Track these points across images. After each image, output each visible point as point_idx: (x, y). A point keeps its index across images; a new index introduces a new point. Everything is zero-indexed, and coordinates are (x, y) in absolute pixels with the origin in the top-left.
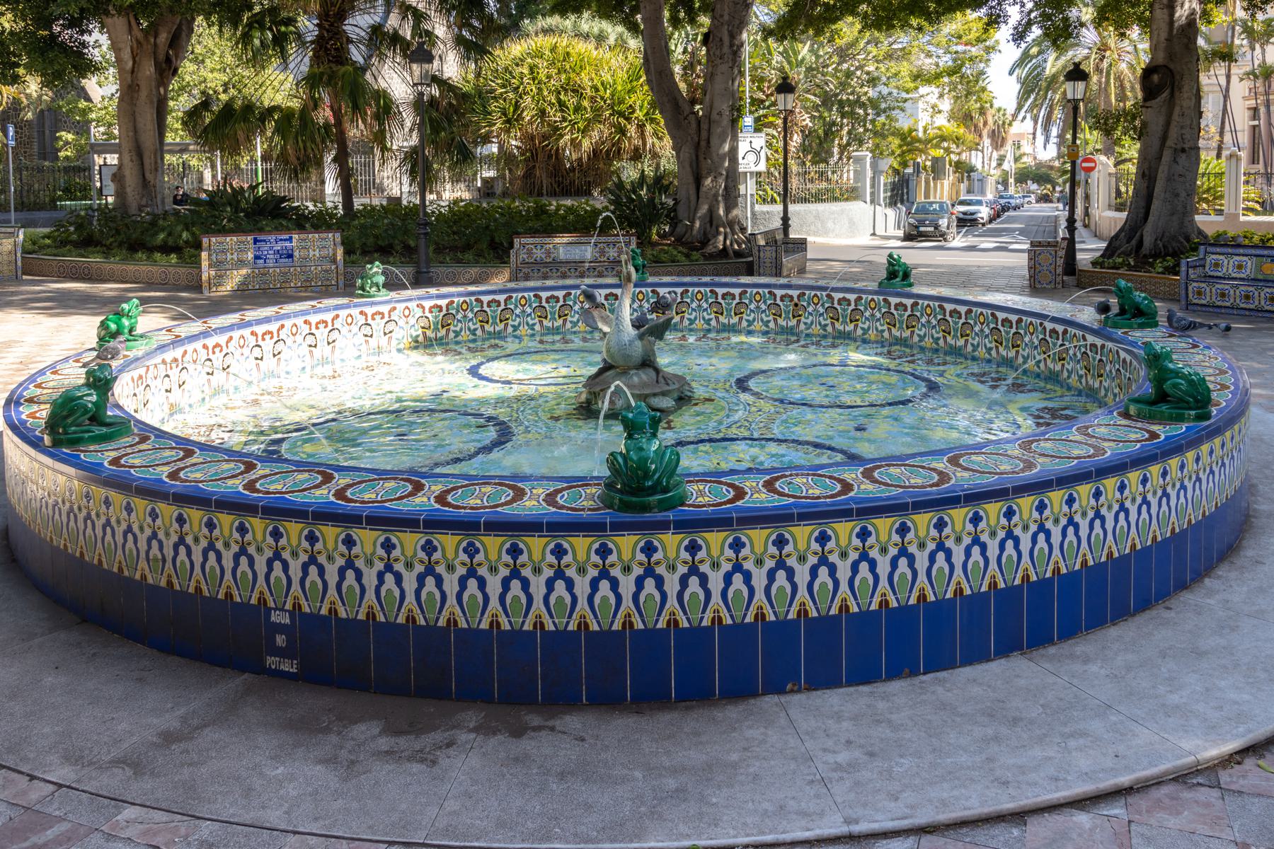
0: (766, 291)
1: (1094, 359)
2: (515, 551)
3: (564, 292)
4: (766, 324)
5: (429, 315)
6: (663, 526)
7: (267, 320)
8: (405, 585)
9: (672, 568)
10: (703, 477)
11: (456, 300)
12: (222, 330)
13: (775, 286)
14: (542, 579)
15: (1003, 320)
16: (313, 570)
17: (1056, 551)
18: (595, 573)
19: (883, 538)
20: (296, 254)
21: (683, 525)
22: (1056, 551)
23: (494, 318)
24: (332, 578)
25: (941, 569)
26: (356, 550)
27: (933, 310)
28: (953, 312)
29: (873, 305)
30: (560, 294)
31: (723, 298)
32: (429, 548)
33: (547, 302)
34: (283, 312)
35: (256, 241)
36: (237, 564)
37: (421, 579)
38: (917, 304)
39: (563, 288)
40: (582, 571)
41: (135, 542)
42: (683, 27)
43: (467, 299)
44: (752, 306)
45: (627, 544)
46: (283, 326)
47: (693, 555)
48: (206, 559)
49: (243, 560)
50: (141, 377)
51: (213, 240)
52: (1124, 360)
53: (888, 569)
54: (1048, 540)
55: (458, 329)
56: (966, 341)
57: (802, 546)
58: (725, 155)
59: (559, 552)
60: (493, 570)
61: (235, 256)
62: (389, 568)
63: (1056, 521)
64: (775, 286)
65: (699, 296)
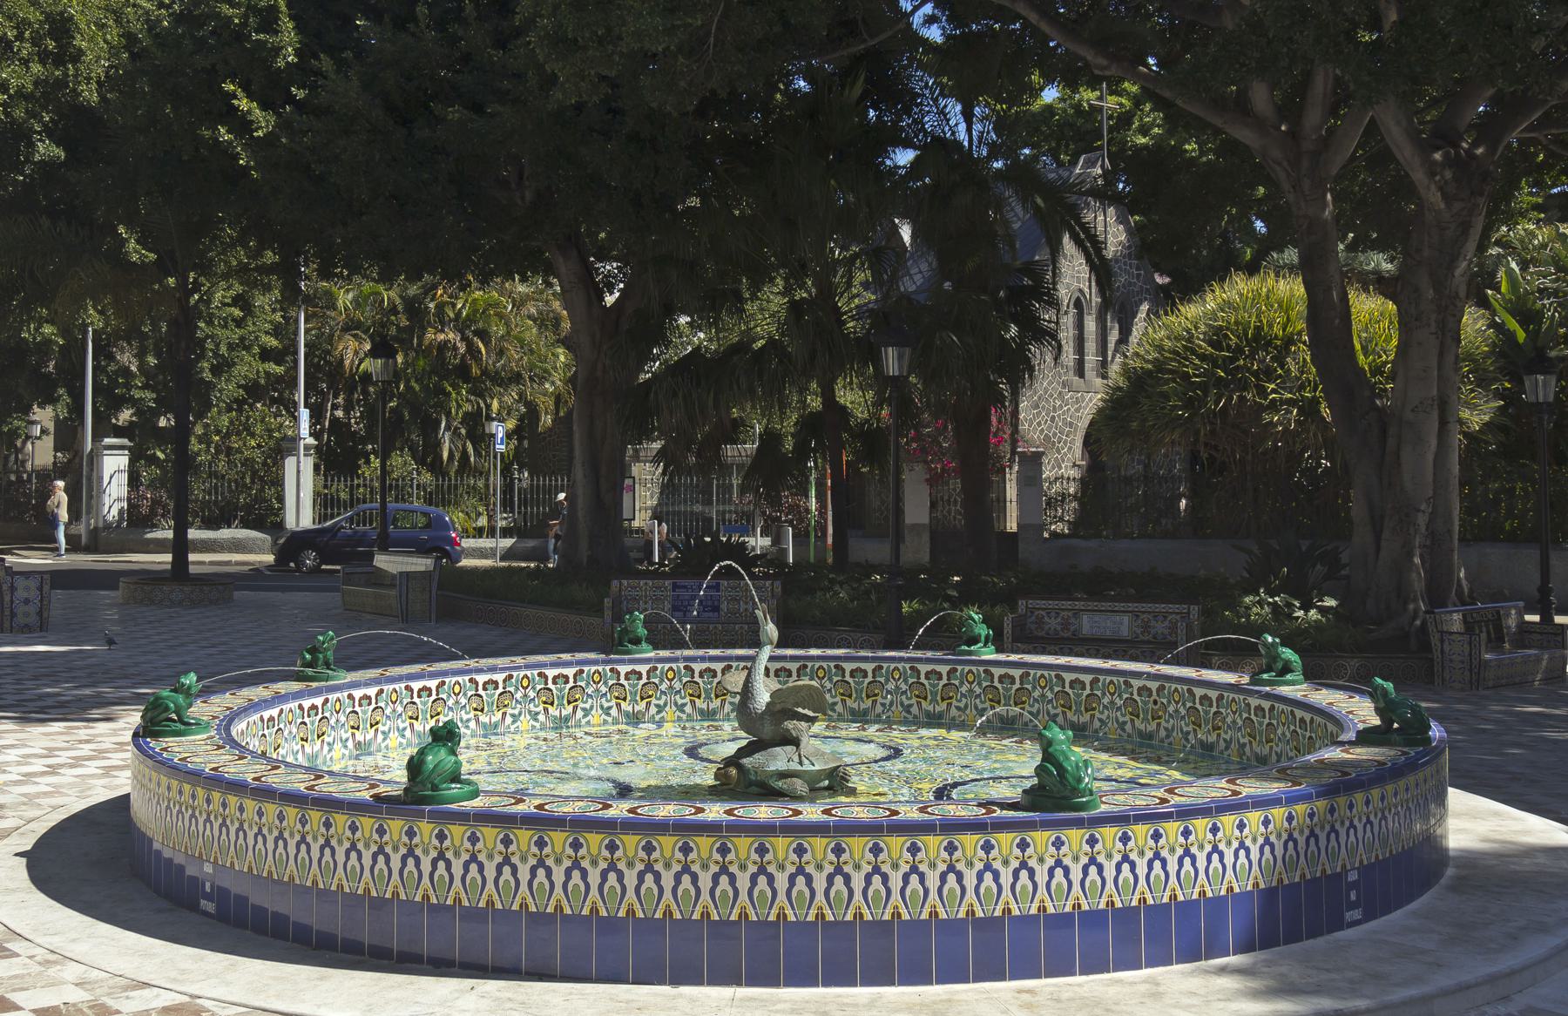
0: (908, 666)
3: (873, 665)
4: (907, 709)
5: (850, 680)
6: (421, 815)
8: (1002, 880)
9: (705, 867)
10: (1460, 831)
11: (515, 674)
13: (544, 665)
14: (748, 875)
16: (381, 858)
17: (1229, 871)
18: (679, 868)
20: (724, 606)
22: (1229, 871)
23: (934, 694)
27: (1182, 696)
28: (1204, 698)
29: (457, 689)
30: (869, 667)
31: (927, 678)
33: (627, 678)
35: (675, 587)
36: (375, 861)
37: (533, 871)
38: (805, 667)
39: (874, 659)
40: (970, 864)
41: (285, 847)
42: (65, 66)
44: (663, 687)
45: (396, 826)
48: (348, 858)
49: (381, 858)
51: (625, 582)
53: (1081, 876)
54: (1248, 856)
55: (661, 702)
56: (1159, 725)
58: (45, 478)
64: (919, 660)
65: (670, 675)
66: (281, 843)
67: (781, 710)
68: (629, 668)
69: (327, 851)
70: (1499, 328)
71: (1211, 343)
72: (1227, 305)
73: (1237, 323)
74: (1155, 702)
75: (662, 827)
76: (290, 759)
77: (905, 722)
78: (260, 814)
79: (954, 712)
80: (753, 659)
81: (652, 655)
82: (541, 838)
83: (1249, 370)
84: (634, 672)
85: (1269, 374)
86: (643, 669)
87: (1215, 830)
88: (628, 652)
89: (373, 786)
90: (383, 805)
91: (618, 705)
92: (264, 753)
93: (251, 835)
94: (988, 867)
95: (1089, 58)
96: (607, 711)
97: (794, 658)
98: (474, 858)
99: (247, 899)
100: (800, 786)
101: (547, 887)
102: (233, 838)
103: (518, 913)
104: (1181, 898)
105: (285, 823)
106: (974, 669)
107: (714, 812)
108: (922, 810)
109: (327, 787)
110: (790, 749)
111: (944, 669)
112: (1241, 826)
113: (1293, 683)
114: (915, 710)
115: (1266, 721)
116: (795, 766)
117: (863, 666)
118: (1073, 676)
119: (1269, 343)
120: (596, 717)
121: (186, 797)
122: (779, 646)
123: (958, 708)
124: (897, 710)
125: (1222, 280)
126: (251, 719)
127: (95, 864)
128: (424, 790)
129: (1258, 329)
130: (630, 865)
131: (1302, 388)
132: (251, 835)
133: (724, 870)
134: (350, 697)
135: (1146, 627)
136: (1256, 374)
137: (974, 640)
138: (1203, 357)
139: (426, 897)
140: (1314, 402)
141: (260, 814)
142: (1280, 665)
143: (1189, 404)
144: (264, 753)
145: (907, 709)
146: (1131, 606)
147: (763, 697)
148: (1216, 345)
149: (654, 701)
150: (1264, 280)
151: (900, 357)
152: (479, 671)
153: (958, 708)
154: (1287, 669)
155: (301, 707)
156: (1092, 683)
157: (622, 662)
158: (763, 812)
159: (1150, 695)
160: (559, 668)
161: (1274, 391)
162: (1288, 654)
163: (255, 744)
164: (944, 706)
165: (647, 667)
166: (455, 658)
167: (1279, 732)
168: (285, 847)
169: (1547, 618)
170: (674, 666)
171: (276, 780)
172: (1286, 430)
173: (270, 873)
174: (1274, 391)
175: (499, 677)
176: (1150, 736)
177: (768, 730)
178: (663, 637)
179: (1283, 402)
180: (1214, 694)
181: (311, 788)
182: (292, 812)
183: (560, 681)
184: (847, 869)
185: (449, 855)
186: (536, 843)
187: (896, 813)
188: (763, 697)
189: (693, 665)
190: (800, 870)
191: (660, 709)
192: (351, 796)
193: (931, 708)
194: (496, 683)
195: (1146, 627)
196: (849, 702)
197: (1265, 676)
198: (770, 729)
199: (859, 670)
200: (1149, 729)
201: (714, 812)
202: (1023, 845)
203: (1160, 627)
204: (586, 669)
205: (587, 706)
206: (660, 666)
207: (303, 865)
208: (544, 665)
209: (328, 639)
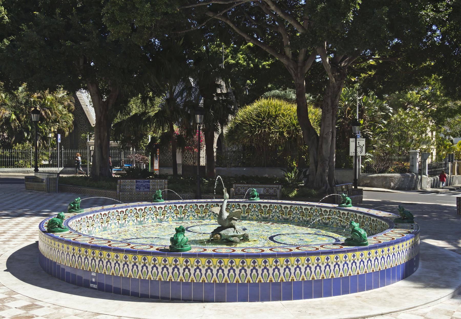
0: (173, 205)
1: (374, 224)
2: (145, 259)
3: (206, 204)
6: (179, 255)
7: (122, 207)
11: (147, 207)
12: (107, 210)
13: (136, 206)
15: (342, 213)
16: (126, 266)
19: (292, 262)
20: (151, 187)
21: (184, 255)
23: (265, 212)
24: (105, 264)
25: (318, 271)
26: (127, 259)
28: (325, 211)
29: (276, 207)
30: (183, 205)
31: (158, 209)
32: (126, 258)
33: (179, 208)
34: (116, 207)
35: (137, 182)
36: (133, 267)
37: (163, 269)
39: (185, 203)
41: (81, 260)
43: (151, 207)
45: (170, 259)
46: (127, 210)
47: (176, 263)
49: (126, 266)
50: (79, 221)
51: (122, 181)
52: (383, 224)
54: (356, 265)
57: (303, 262)
59: (155, 260)
60: (248, 267)
61: (129, 187)
62: (117, 262)
63: (350, 261)
64: (240, 202)
66: (80, 258)
67: (230, 218)
68: (159, 206)
69: (93, 261)
70: (222, 128)
71: (256, 116)
72: (261, 106)
73: (263, 111)
74: (309, 212)
75: (225, 256)
76: (84, 233)
77: (256, 220)
78: (80, 251)
79: (250, 216)
80: (223, 202)
81: (164, 202)
82: (145, 258)
83: (266, 123)
84: (160, 207)
85: (271, 124)
86: (163, 206)
87: (369, 254)
88: (158, 202)
89: (109, 242)
90: (163, 252)
91: (176, 215)
92: (77, 231)
93: (77, 257)
94: (298, 266)
95: (245, 37)
96: (153, 219)
97: (205, 202)
98: (145, 265)
99: (82, 277)
100: (237, 239)
101: (146, 272)
102: (77, 259)
103: (148, 280)
104: (335, 277)
105: (81, 253)
106: (256, 204)
107: (210, 249)
108: (271, 250)
109: (95, 242)
110: (233, 229)
111: (247, 204)
112: (376, 253)
113: (350, 206)
114: (260, 216)
115: (362, 220)
116: (236, 234)
117: (203, 204)
118: (285, 206)
119: (271, 117)
120: (150, 221)
121: (56, 246)
122: (229, 198)
123: (251, 215)
124: (255, 217)
125: (258, 100)
126: (73, 221)
127: (30, 266)
128: (175, 247)
129: (269, 113)
130: (170, 266)
131: (280, 128)
132: (77, 257)
133: (220, 268)
134: (101, 214)
135: (268, 191)
136: (268, 124)
137: (254, 196)
138: (255, 120)
139: (140, 277)
140: (283, 132)
141: (80, 251)
142: (347, 202)
143: (251, 132)
144: (77, 231)
145: (258, 216)
146: (264, 186)
147: (226, 215)
148: (259, 117)
149: (250, 213)
150: (270, 100)
151: (201, 118)
152: (119, 208)
153: (251, 215)
154: (348, 203)
155: (87, 217)
156: (290, 207)
157: (157, 204)
158: (224, 249)
159: (308, 210)
160: (121, 207)
161: (273, 129)
162: (348, 199)
163: (74, 228)
164: (247, 214)
165: (206, 204)
166: (119, 203)
167: (366, 223)
168: (81, 260)
169: (356, 187)
170: (171, 205)
171: (80, 240)
172: (276, 139)
173: (77, 267)
174: (273, 129)
175: (143, 208)
176: (327, 224)
177: (227, 224)
178: (168, 197)
179: (275, 132)
180: (362, 215)
181: (90, 242)
182: (83, 249)
183: (140, 210)
184: (268, 267)
185: (137, 264)
186: (143, 259)
187: (263, 251)
188: (226, 215)
189: (177, 205)
190: (265, 268)
191: (209, 216)
192: (103, 245)
193: (264, 216)
194: (142, 209)
195: (268, 191)
196: (262, 215)
197: (343, 205)
198: (225, 224)
199: (265, 206)
200: (327, 222)
201: (210, 249)
202: (298, 261)
203: (271, 191)
204: (147, 207)
205: (188, 215)
206: (167, 205)
207: (135, 272)
208: (136, 206)
209: (79, 200)
